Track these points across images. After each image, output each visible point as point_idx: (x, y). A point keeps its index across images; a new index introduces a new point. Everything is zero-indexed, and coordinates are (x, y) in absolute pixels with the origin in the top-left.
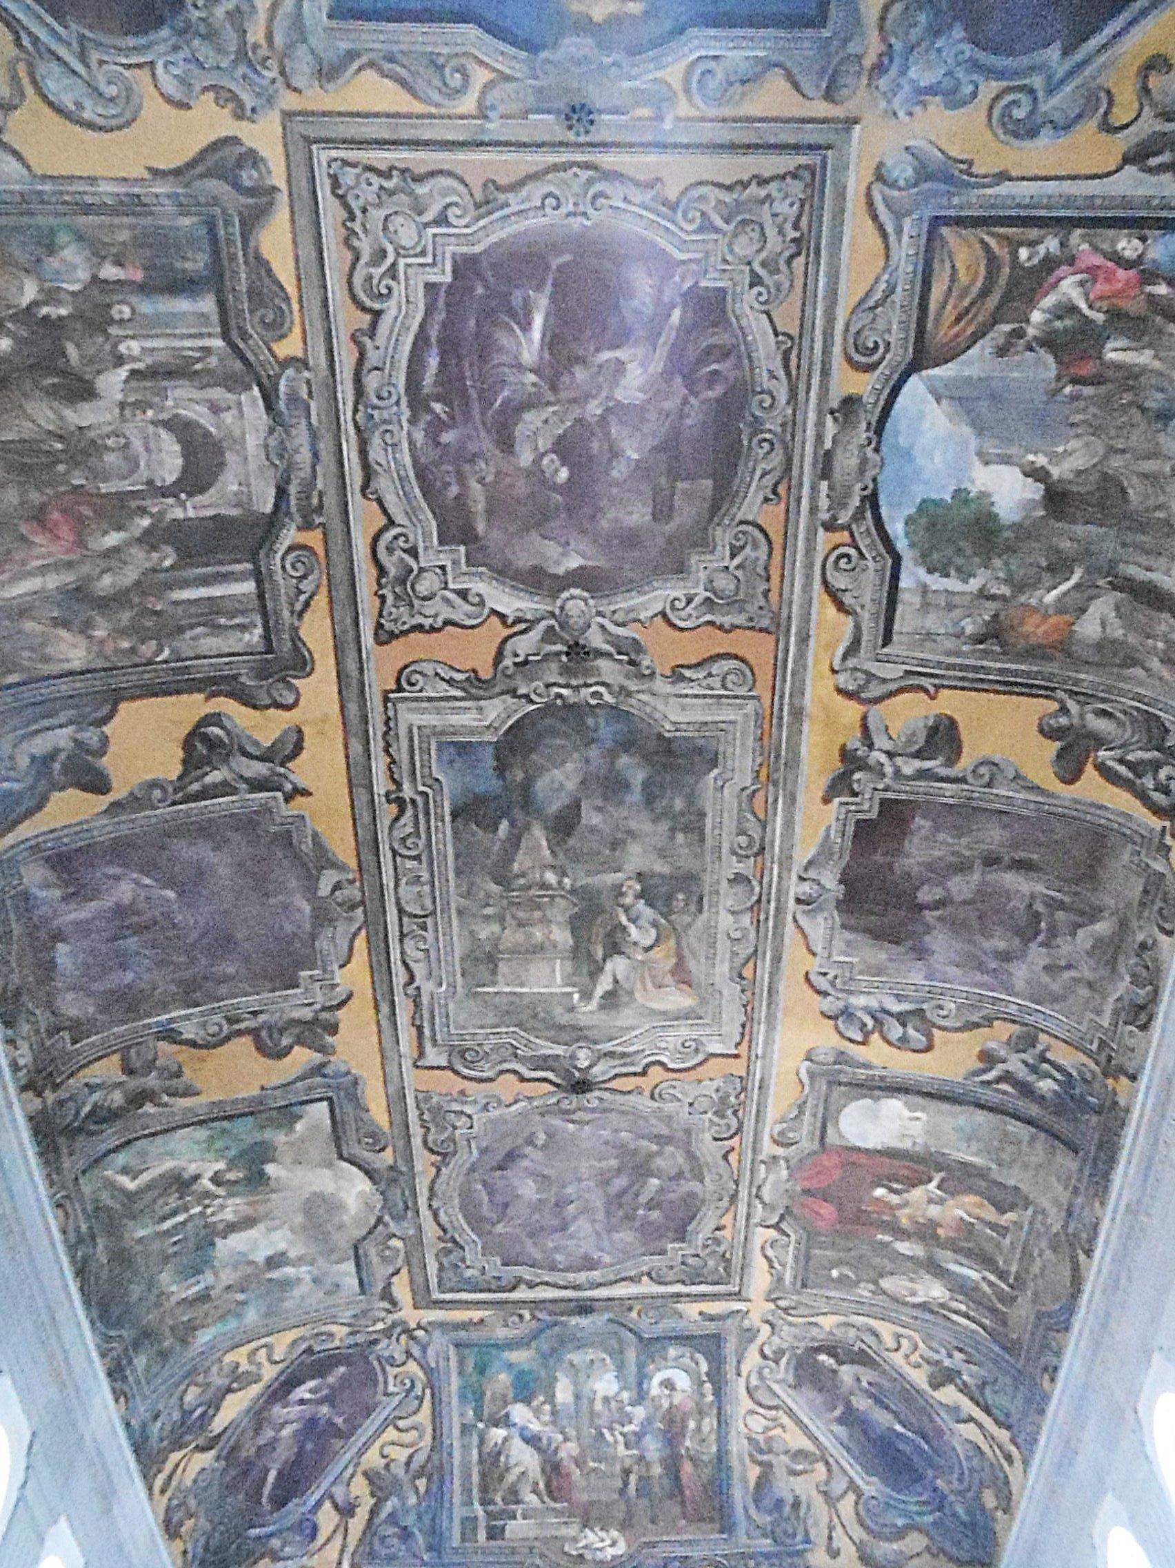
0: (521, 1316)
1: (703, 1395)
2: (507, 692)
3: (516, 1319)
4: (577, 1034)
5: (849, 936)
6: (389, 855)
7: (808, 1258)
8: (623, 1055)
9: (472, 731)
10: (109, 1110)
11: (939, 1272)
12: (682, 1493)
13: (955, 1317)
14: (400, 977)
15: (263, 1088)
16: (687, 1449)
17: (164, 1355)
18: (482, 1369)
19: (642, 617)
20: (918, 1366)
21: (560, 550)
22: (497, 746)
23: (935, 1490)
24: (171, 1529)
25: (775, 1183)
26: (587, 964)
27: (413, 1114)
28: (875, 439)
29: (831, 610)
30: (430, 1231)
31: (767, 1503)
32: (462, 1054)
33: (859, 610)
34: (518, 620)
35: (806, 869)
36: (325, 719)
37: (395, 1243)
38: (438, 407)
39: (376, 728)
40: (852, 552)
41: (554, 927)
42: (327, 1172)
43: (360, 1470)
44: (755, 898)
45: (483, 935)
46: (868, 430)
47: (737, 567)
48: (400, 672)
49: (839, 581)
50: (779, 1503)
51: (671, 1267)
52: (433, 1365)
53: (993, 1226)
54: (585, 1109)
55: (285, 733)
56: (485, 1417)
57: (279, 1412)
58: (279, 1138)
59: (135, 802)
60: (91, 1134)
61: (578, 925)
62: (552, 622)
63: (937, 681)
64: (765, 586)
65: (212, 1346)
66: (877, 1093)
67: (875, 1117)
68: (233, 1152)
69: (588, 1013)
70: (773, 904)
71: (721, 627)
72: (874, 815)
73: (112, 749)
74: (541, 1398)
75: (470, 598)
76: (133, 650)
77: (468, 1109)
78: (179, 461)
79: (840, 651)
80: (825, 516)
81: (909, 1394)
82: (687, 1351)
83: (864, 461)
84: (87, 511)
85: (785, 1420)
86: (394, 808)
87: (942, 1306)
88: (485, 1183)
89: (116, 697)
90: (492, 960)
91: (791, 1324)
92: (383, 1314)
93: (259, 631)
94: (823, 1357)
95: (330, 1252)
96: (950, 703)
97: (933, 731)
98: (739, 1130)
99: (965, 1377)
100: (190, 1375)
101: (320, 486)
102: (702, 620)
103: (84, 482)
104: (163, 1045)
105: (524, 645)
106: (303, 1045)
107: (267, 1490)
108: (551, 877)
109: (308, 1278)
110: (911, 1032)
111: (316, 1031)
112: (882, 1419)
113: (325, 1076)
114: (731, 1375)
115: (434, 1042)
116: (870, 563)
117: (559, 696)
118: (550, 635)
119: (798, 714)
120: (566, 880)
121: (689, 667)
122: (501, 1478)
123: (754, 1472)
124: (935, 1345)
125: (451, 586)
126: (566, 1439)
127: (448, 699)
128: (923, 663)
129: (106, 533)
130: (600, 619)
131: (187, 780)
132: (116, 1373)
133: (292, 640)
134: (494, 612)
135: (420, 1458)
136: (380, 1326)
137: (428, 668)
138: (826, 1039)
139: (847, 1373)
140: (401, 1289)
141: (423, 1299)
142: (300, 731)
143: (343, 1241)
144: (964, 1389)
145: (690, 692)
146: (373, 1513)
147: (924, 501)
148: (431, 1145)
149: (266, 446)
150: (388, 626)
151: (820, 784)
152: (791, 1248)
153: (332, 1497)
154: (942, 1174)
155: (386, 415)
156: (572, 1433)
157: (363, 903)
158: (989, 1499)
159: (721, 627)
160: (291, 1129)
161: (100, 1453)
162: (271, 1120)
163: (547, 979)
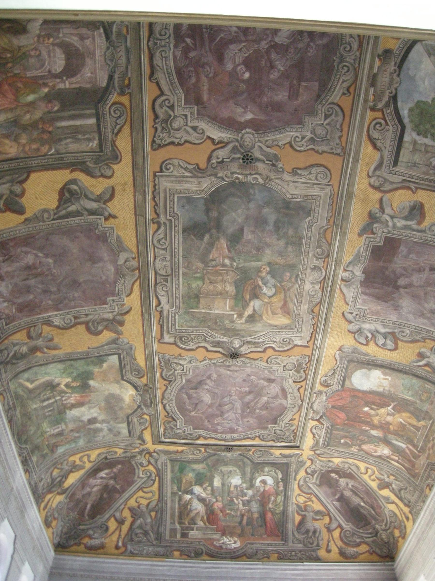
0: (200, 451)
1: (278, 487)
2: (212, 175)
3: (198, 452)
4: (234, 333)
5: (364, 297)
6: (152, 247)
7: (331, 434)
8: (255, 343)
9: (195, 192)
10: (22, 354)
11: (387, 443)
12: (266, 525)
13: (393, 462)
14: (154, 302)
15: (89, 348)
16: (270, 508)
17: (44, 456)
18: (182, 470)
19: (280, 144)
20: (374, 480)
21: (243, 110)
22: (205, 199)
23: (374, 528)
24: (47, 524)
25: (320, 403)
26: (240, 301)
27: (156, 363)
28: (398, 70)
29: (370, 148)
30: (162, 413)
31: (303, 530)
32: (181, 339)
33: (383, 148)
34: (220, 142)
35: (347, 266)
36: (126, 183)
37: (145, 417)
38: (188, 40)
39: (149, 189)
40: (383, 122)
41: (227, 284)
42: (116, 385)
43: (127, 507)
44: (322, 277)
45: (194, 285)
46: (395, 66)
47: (327, 124)
48: (163, 162)
49: (375, 135)
50: (307, 531)
51: (269, 435)
52: (160, 467)
53: (413, 426)
54: (237, 366)
55: (106, 189)
56: (182, 489)
57: (92, 481)
58: (96, 370)
59: (37, 218)
60: (13, 364)
61: (238, 284)
62: (237, 144)
63: (416, 186)
64: (339, 134)
65: (64, 454)
66: (370, 367)
67: (368, 377)
68: (75, 374)
69: (240, 323)
70: (330, 281)
71: (317, 152)
72: (381, 244)
73: (27, 195)
74: (207, 484)
75: (198, 131)
76: (38, 150)
77: (182, 362)
78: (64, 62)
79: (373, 167)
80: (371, 104)
81: (369, 492)
82: (273, 469)
83: (392, 79)
84: (20, 85)
85: (314, 499)
86: (156, 226)
87: (388, 457)
88: (187, 394)
89: (29, 171)
90: (197, 297)
91: (320, 461)
92: (138, 445)
93: (96, 142)
94: (333, 475)
95: (116, 419)
96: (422, 196)
97: (413, 208)
98: (305, 379)
99: (394, 486)
100: (55, 465)
101: (130, 75)
102: (308, 147)
103: (19, 71)
104: (45, 327)
105: (222, 154)
106: (108, 330)
107: (87, 511)
108: (227, 262)
109: (106, 428)
110: (388, 342)
111: (115, 323)
112: (356, 500)
113: (116, 344)
114: (292, 480)
115: (168, 332)
116: (391, 128)
117: (238, 178)
118: (234, 150)
119: (350, 195)
120: (235, 264)
121: (300, 169)
122: (188, 514)
123: (298, 519)
124: (382, 472)
125: (189, 124)
126: (217, 501)
127: (183, 177)
128: (411, 177)
129: (28, 95)
130: (259, 144)
131: (60, 209)
132: (25, 462)
133: (112, 146)
134: (209, 138)
135: (154, 504)
136: (137, 450)
137: (176, 162)
138: (349, 342)
139: (343, 482)
140: (147, 436)
141: (157, 440)
142: (113, 189)
143: (122, 415)
144: (393, 491)
145: (299, 180)
146: (132, 524)
147: (418, 102)
148: (164, 377)
149: (105, 55)
150: (158, 141)
151: (357, 230)
152: (324, 429)
153: (114, 516)
154: (395, 403)
155: (163, 43)
156: (220, 498)
157: (138, 268)
158: (397, 533)
159: (317, 152)
160: (101, 366)
161: (19, 493)
162: (92, 362)
163: (223, 308)
